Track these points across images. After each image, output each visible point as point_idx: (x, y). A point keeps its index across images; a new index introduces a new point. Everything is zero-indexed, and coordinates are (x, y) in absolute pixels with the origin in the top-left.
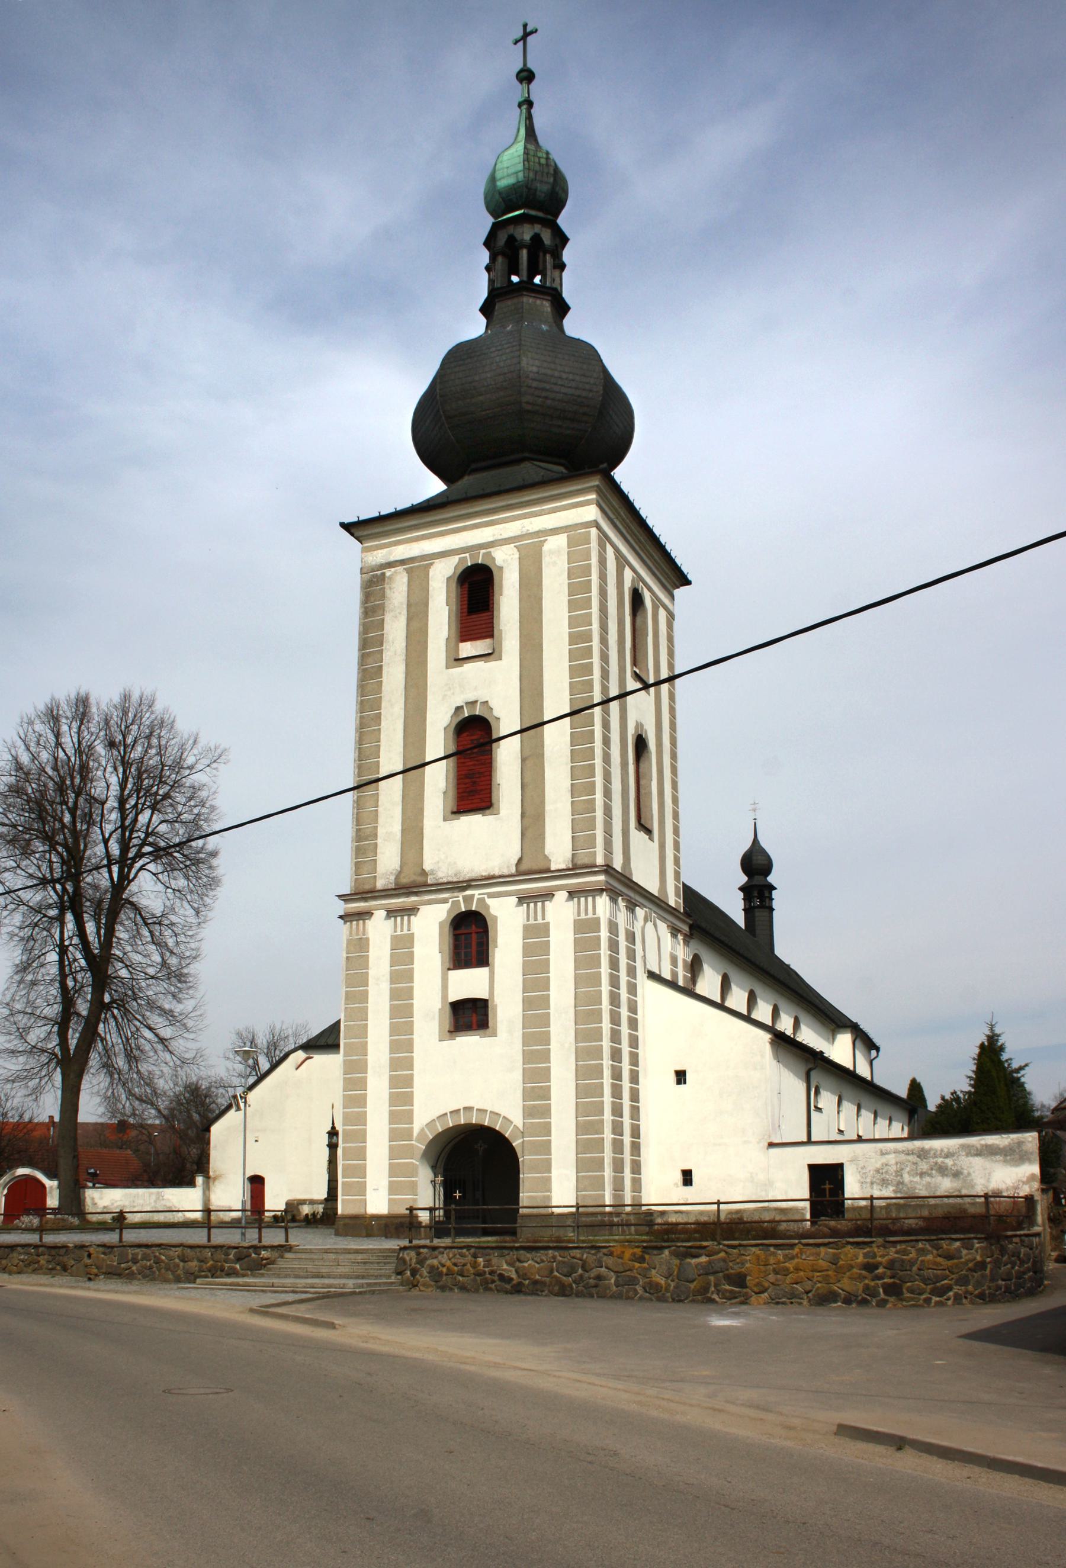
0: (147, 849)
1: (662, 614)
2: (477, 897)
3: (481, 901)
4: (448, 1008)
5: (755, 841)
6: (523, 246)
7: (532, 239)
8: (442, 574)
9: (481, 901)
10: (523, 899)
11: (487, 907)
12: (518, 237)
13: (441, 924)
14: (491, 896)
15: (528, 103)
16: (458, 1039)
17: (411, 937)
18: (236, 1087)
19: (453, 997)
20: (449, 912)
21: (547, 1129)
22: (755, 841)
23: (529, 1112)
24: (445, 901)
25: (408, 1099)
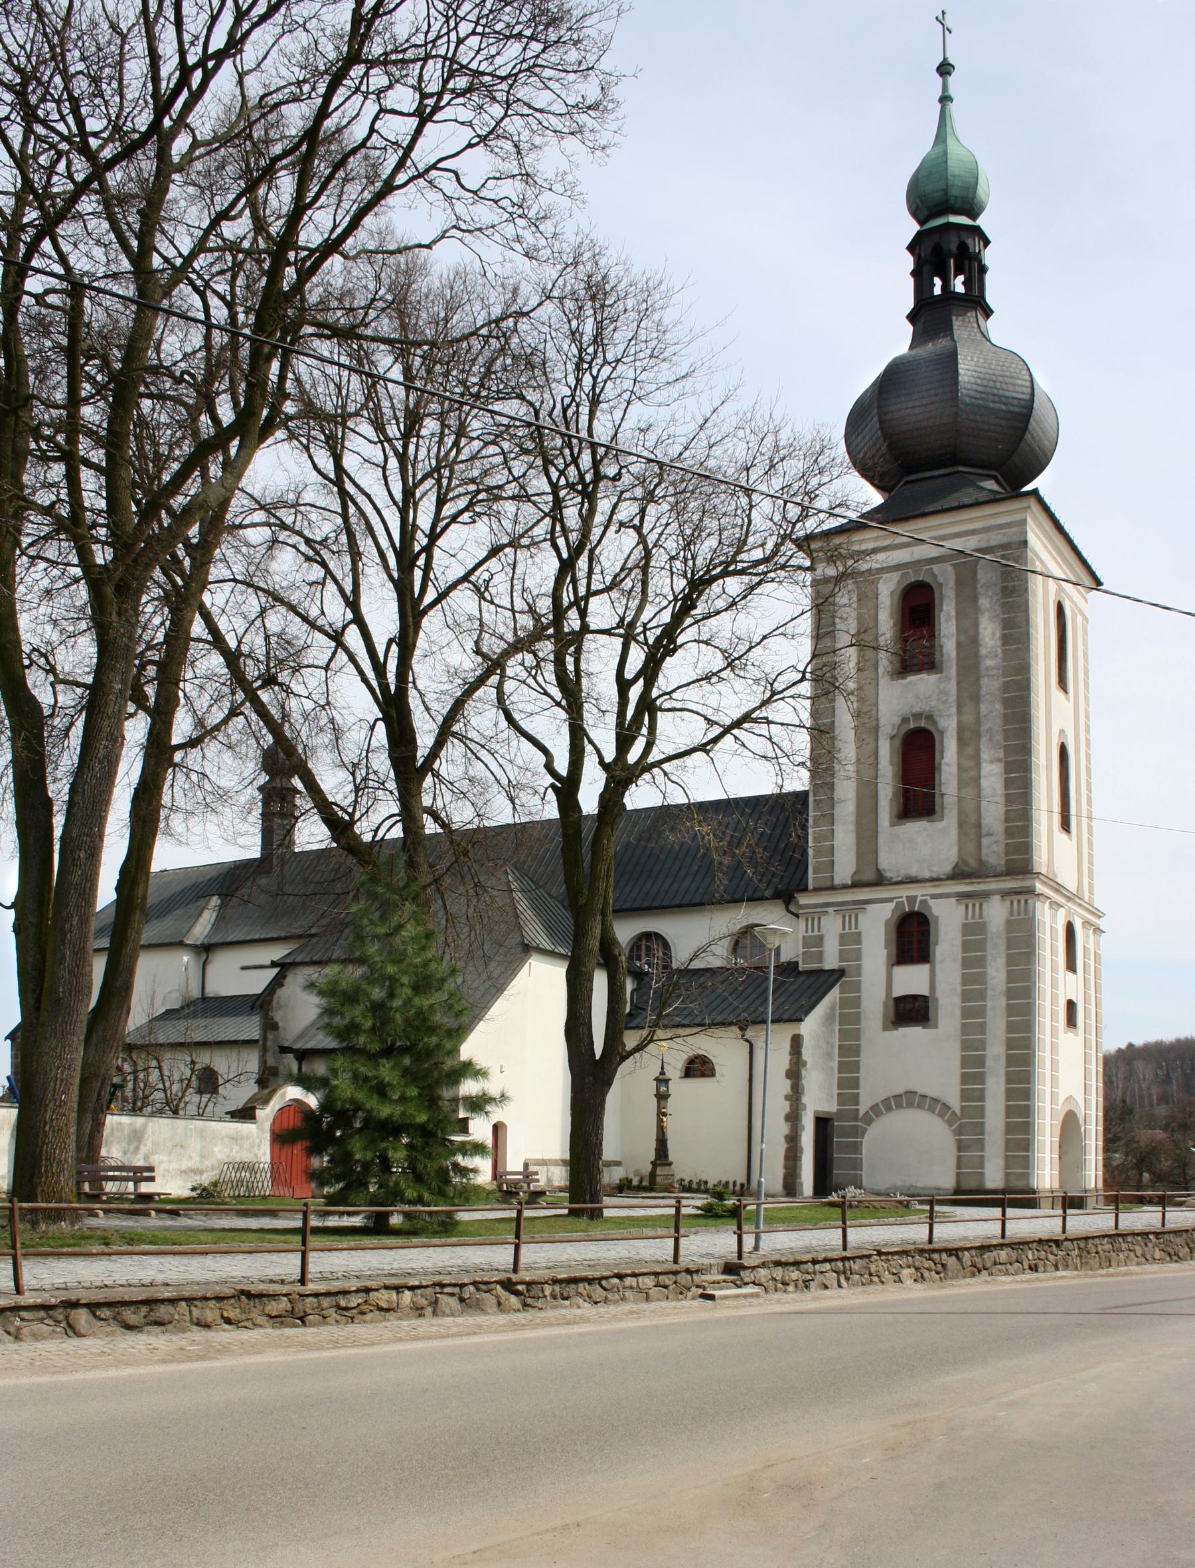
0: (533, 672)
1: (1079, 619)
2: (919, 898)
3: (924, 902)
4: (891, 1004)
5: (945, 59)
6: (950, 256)
7: (958, 248)
8: (887, 590)
9: (924, 902)
10: (962, 896)
11: (929, 908)
12: (944, 246)
13: (887, 923)
14: (934, 896)
15: (945, 99)
16: (901, 1029)
17: (859, 935)
18: (259, 65)
19: (897, 993)
20: (893, 911)
21: (981, 1111)
22: (945, 59)
23: (965, 1096)
24: (890, 900)
25: (855, 1083)
